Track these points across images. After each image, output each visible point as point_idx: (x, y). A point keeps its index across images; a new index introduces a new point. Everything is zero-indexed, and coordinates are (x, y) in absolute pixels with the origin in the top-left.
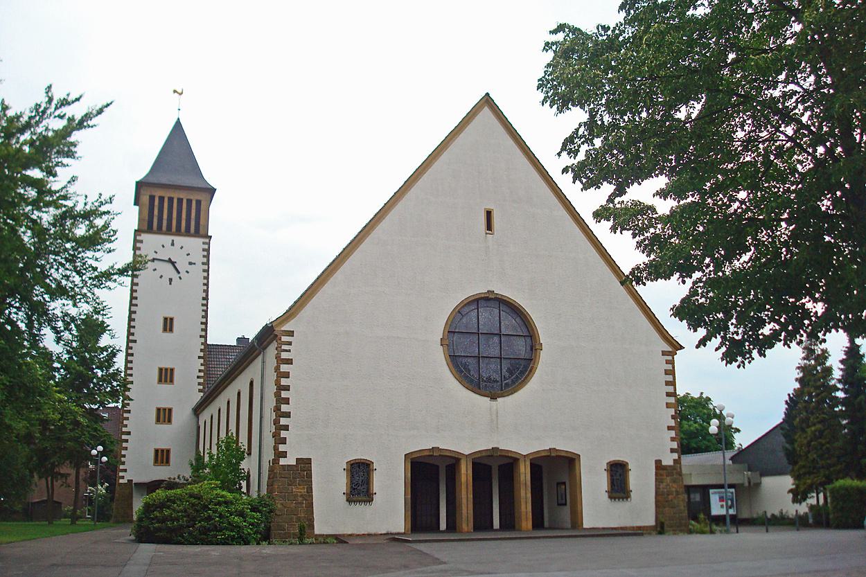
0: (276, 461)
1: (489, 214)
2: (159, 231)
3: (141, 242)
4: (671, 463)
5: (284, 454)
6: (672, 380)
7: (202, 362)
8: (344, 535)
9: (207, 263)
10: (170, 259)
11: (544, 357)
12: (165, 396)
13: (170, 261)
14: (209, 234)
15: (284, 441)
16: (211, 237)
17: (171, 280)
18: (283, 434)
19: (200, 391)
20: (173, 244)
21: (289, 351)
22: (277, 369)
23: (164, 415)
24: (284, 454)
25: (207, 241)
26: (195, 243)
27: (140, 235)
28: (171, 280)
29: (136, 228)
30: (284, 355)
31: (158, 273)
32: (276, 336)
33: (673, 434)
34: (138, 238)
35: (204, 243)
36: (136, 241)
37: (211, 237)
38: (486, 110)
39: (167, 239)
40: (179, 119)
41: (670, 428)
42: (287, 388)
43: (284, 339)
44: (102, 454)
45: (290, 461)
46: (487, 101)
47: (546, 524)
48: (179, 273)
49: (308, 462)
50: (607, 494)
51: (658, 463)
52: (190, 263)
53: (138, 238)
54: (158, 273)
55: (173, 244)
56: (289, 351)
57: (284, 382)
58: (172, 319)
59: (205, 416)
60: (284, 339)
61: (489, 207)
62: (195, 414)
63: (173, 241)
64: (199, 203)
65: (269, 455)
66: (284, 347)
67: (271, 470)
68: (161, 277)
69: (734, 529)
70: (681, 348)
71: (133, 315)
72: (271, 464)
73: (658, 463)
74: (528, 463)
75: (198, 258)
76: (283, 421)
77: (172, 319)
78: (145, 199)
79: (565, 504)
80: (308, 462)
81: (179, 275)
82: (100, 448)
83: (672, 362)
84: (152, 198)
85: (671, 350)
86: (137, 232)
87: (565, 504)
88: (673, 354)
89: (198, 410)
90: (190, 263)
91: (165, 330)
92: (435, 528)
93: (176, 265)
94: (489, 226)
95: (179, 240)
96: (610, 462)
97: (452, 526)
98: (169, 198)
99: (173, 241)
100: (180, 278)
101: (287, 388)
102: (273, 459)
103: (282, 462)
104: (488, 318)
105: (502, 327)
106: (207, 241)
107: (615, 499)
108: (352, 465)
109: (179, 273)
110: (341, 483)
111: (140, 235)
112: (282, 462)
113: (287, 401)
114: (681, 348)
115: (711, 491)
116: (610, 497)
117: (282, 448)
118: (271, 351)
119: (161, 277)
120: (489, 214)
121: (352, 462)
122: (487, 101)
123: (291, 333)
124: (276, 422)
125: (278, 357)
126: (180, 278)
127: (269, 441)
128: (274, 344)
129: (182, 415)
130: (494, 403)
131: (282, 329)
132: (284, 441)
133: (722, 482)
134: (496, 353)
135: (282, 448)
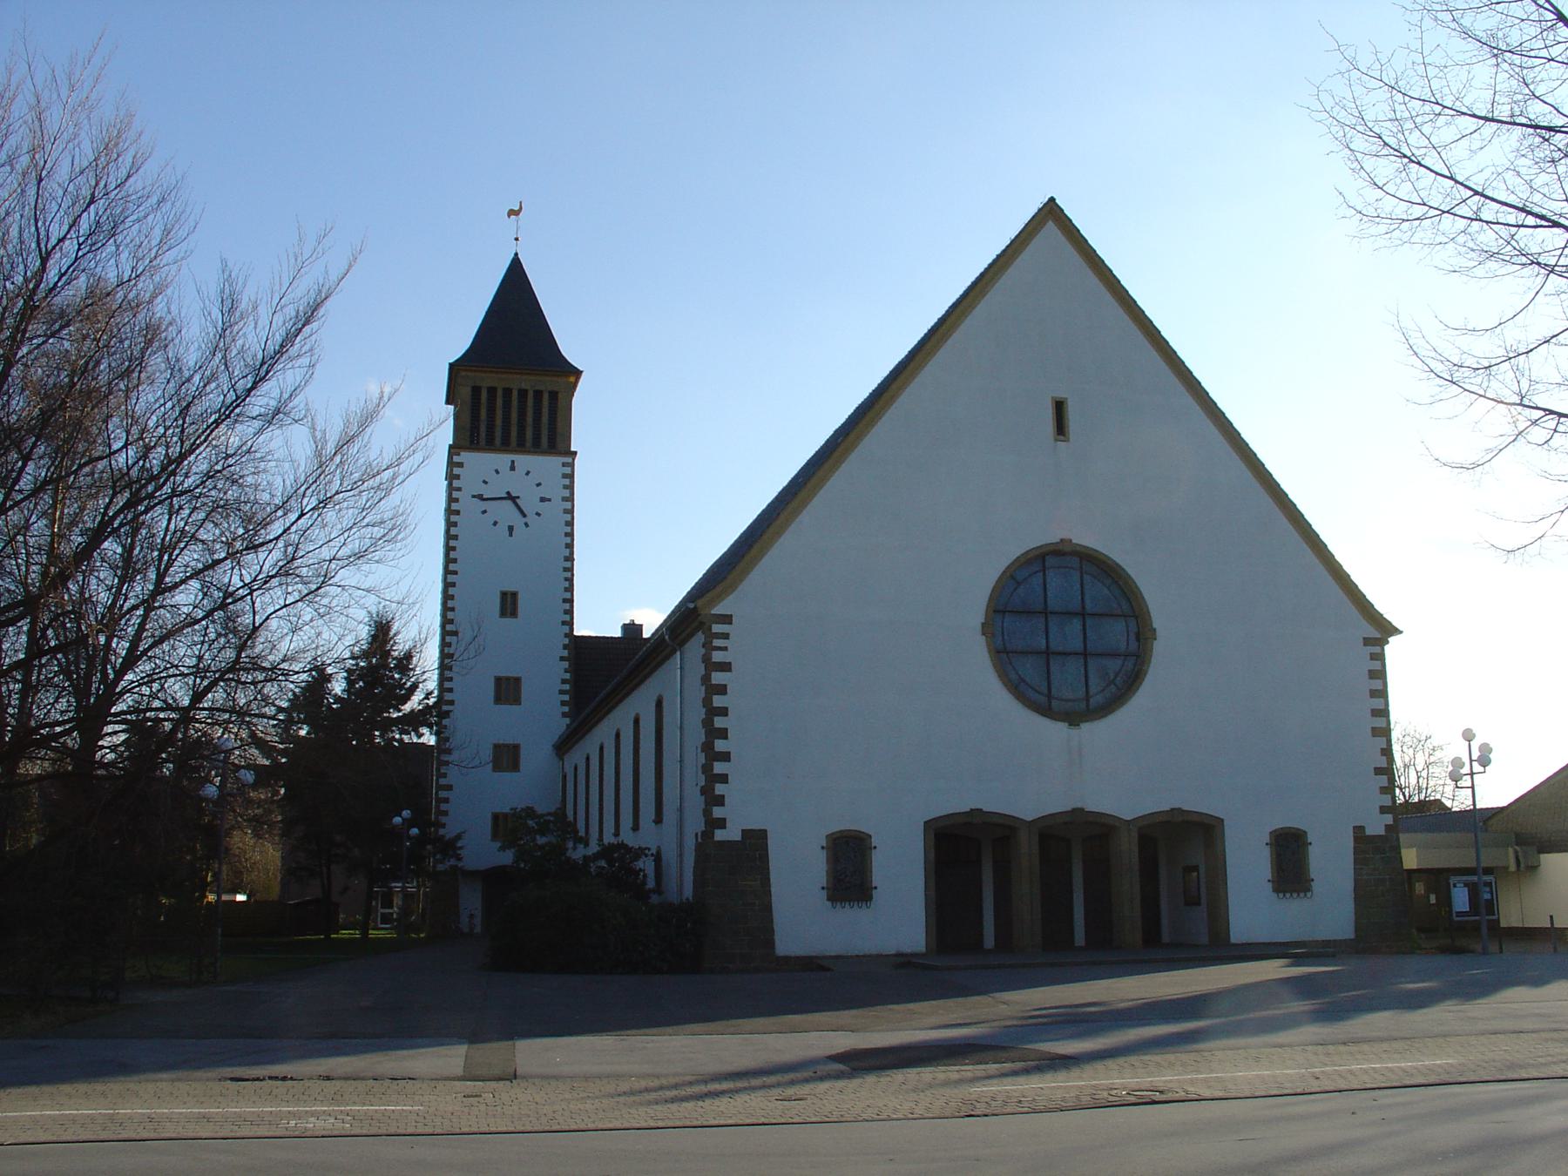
0: (707, 834)
1: (1059, 407)
2: (490, 446)
3: (460, 465)
4: (1381, 831)
5: (721, 824)
6: (451, 541)
7: (567, 666)
8: (825, 957)
9: (571, 499)
10: (508, 493)
11: (1160, 649)
12: (506, 724)
13: (510, 497)
14: (573, 449)
15: (720, 800)
16: (575, 453)
17: (511, 529)
18: (720, 789)
19: (564, 715)
20: (513, 468)
21: (725, 649)
22: (706, 679)
23: (507, 757)
24: (721, 824)
25: (570, 460)
26: (553, 463)
27: (459, 455)
28: (511, 529)
29: (451, 443)
30: (717, 657)
31: (489, 518)
32: (702, 624)
33: (566, 664)
34: (456, 459)
35: (564, 465)
36: (451, 464)
37: (575, 453)
38: (1051, 227)
39: (503, 459)
40: (516, 254)
41: (562, 659)
42: (723, 712)
43: (717, 628)
44: (409, 823)
45: (731, 833)
46: (1051, 212)
47: (1166, 938)
48: (524, 515)
49: (761, 835)
50: (1270, 884)
51: (1359, 831)
52: (543, 500)
53: (456, 459)
54: (489, 518)
55: (513, 468)
56: (725, 649)
57: (718, 701)
58: (514, 595)
59: (576, 757)
60: (717, 628)
61: (1061, 395)
62: (557, 754)
63: (513, 462)
64: (554, 396)
65: (695, 824)
66: (717, 643)
67: (699, 848)
68: (495, 523)
69: (1494, 947)
70: (1396, 631)
71: (450, 589)
72: (700, 840)
73: (1359, 831)
74: (1135, 834)
75: (556, 492)
76: (719, 768)
77: (514, 595)
78: (465, 392)
79: (1199, 904)
80: (761, 835)
81: (524, 520)
82: (406, 813)
83: (1380, 657)
84: (476, 391)
85: (1379, 636)
86: (454, 450)
87: (1199, 904)
88: (1382, 642)
89: (563, 746)
90: (543, 500)
91: (503, 614)
92: (977, 946)
93: (518, 501)
94: (1061, 428)
95: (524, 461)
96: (1275, 831)
97: (1005, 940)
98: (504, 389)
99: (513, 462)
100: (526, 525)
101: (723, 712)
102: (703, 832)
103: (720, 835)
104: (1061, 587)
105: (1088, 602)
106: (570, 460)
107: (1284, 892)
108: (835, 839)
109: (524, 515)
110: (816, 868)
111: (459, 455)
112: (720, 835)
113: (723, 734)
114: (1396, 631)
115: (1453, 880)
116: (1277, 890)
117: (717, 812)
118: (695, 647)
119: (495, 523)
120: (1059, 407)
121: (835, 836)
122: (1051, 212)
123: (727, 619)
124: (707, 769)
125: (706, 659)
126: (526, 525)
127: (695, 802)
128: (700, 638)
129: (537, 756)
130: (1074, 732)
131: (713, 612)
132: (720, 800)
133: (1474, 864)
134: (1077, 645)
135: (717, 812)
